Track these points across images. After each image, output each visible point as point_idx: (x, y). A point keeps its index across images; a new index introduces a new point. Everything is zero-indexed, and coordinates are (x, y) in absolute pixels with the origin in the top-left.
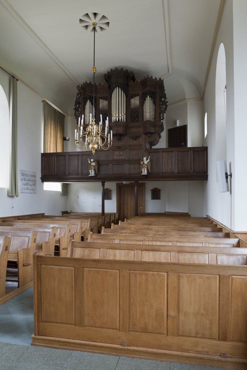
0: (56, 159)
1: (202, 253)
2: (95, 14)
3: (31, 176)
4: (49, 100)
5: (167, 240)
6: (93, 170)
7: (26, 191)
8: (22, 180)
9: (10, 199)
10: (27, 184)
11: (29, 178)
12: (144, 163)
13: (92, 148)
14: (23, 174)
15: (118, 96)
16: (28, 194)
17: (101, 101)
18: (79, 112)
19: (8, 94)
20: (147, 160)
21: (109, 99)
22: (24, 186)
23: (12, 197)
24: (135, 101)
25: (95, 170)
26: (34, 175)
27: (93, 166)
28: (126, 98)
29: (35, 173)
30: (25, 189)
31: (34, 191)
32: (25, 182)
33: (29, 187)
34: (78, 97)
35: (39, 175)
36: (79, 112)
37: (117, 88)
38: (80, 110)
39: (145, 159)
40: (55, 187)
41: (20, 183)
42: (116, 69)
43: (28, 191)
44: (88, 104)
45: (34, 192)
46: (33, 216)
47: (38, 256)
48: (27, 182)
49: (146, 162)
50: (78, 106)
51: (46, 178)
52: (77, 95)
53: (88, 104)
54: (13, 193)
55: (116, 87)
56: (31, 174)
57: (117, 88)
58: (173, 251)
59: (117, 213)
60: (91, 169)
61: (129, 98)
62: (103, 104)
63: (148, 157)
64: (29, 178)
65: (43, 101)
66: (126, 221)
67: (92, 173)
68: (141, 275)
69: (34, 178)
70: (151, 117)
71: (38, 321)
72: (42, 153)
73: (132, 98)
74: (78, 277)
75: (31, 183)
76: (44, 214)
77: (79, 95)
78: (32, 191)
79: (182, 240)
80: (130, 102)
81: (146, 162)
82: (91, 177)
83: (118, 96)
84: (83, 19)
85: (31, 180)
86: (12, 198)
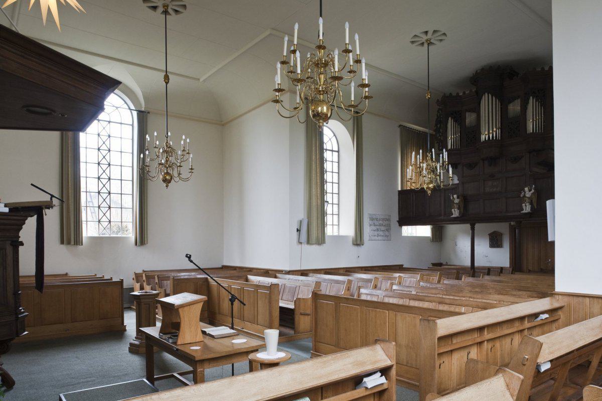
0: (414, 197)
1: (459, 305)
2: (426, 33)
3: (383, 220)
4: (411, 124)
5: (460, 295)
6: (456, 209)
7: (376, 238)
8: (370, 225)
9: (356, 248)
10: (377, 230)
11: (381, 222)
12: (524, 196)
13: (427, 188)
14: (372, 219)
15: (488, 105)
16: (380, 241)
17: (467, 114)
18: (441, 134)
19: (352, 135)
20: (530, 190)
21: (477, 110)
22: (374, 232)
23: (357, 245)
24: (514, 108)
25: (459, 209)
26: (387, 218)
27: (456, 203)
28: (501, 105)
29: (390, 216)
30: (374, 236)
31: (388, 238)
32: (375, 228)
33: (381, 233)
34: (438, 114)
35: (395, 217)
36: (441, 134)
37: (486, 94)
38: (441, 130)
39: (526, 189)
40: (425, 231)
41: (367, 230)
42: (483, 69)
43: (380, 238)
44: (450, 123)
45: (387, 239)
46: (386, 268)
47: (315, 293)
48: (378, 227)
49: (528, 194)
50: (439, 126)
51: (405, 220)
52: (438, 112)
53: (450, 123)
54: (358, 241)
55: (485, 93)
56: (382, 217)
57: (486, 94)
58: (435, 302)
59: (510, 267)
60: (454, 208)
61: (504, 103)
62: (470, 118)
63: (531, 187)
64: (381, 222)
65: (400, 126)
66: (483, 277)
67: (456, 213)
68: (372, 311)
69: (387, 222)
70: (539, 126)
71: (315, 342)
72: (399, 191)
73: (510, 102)
74: (337, 308)
75: (383, 228)
76: (402, 265)
77: (440, 111)
78: (384, 238)
79: (475, 296)
80: (507, 109)
81: (528, 194)
82: (455, 218)
83: (488, 105)
84: (413, 40)
85: (384, 224)
86: (359, 247)
